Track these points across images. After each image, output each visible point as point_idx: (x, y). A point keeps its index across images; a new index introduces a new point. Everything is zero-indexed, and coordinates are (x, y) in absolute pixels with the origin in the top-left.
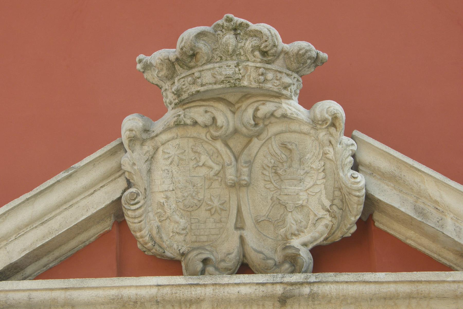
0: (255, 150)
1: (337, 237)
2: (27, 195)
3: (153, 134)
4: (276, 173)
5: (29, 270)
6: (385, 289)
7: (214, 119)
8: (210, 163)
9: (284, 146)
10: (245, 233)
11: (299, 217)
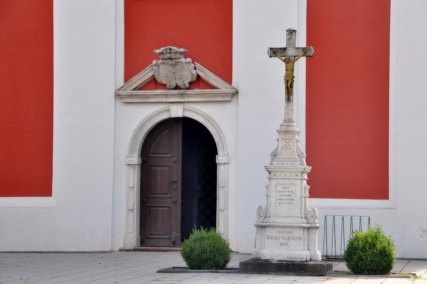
1: (193, 81)
3: (158, 64)
4: (181, 71)
6: (198, 93)
8: (169, 69)
11: (185, 78)
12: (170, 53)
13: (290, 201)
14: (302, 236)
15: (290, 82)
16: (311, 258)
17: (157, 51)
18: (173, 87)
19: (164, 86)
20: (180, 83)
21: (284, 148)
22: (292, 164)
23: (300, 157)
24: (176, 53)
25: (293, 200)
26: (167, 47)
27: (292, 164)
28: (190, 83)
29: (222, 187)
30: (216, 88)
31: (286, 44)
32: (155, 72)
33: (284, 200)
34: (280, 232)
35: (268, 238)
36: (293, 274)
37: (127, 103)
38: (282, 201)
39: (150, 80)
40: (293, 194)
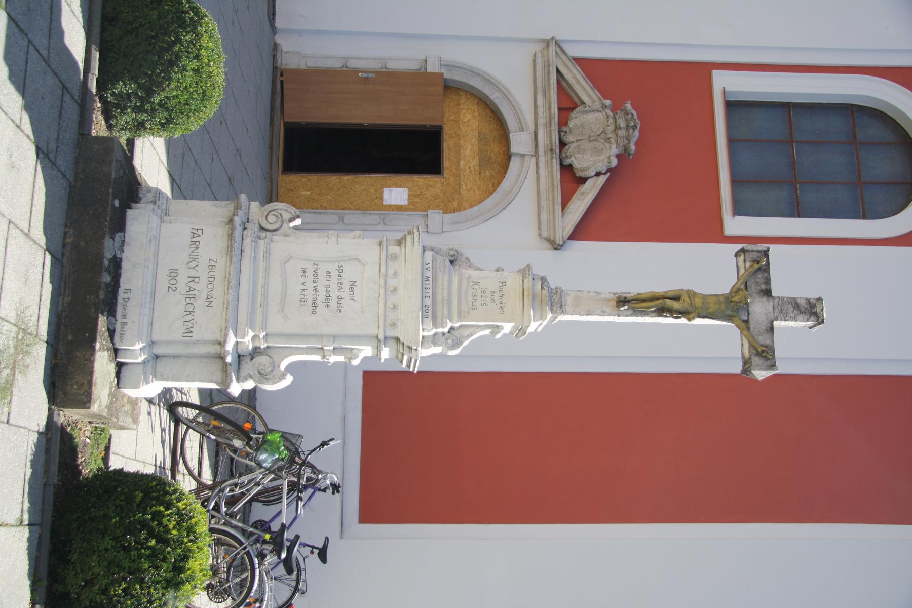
0: (601, 141)
1: (575, 171)
2: (584, 75)
5: (559, 76)
7: (609, 126)
9: (602, 149)
10: (575, 143)
12: (627, 127)
13: (310, 302)
14: (196, 336)
15: (676, 305)
16: (129, 366)
17: (628, 106)
18: (562, 138)
19: (563, 122)
20: (571, 149)
21: (476, 287)
22: (427, 311)
23: (446, 336)
24: (628, 138)
25: (314, 312)
26: (637, 120)
27: (427, 311)
28: (570, 166)
29: (385, 221)
30: (563, 209)
31: (781, 296)
32: (589, 107)
33: (315, 284)
34: (212, 268)
35: (195, 231)
36: (65, 305)
37: (534, 61)
38: (311, 278)
39: (574, 100)
40: (331, 311)
